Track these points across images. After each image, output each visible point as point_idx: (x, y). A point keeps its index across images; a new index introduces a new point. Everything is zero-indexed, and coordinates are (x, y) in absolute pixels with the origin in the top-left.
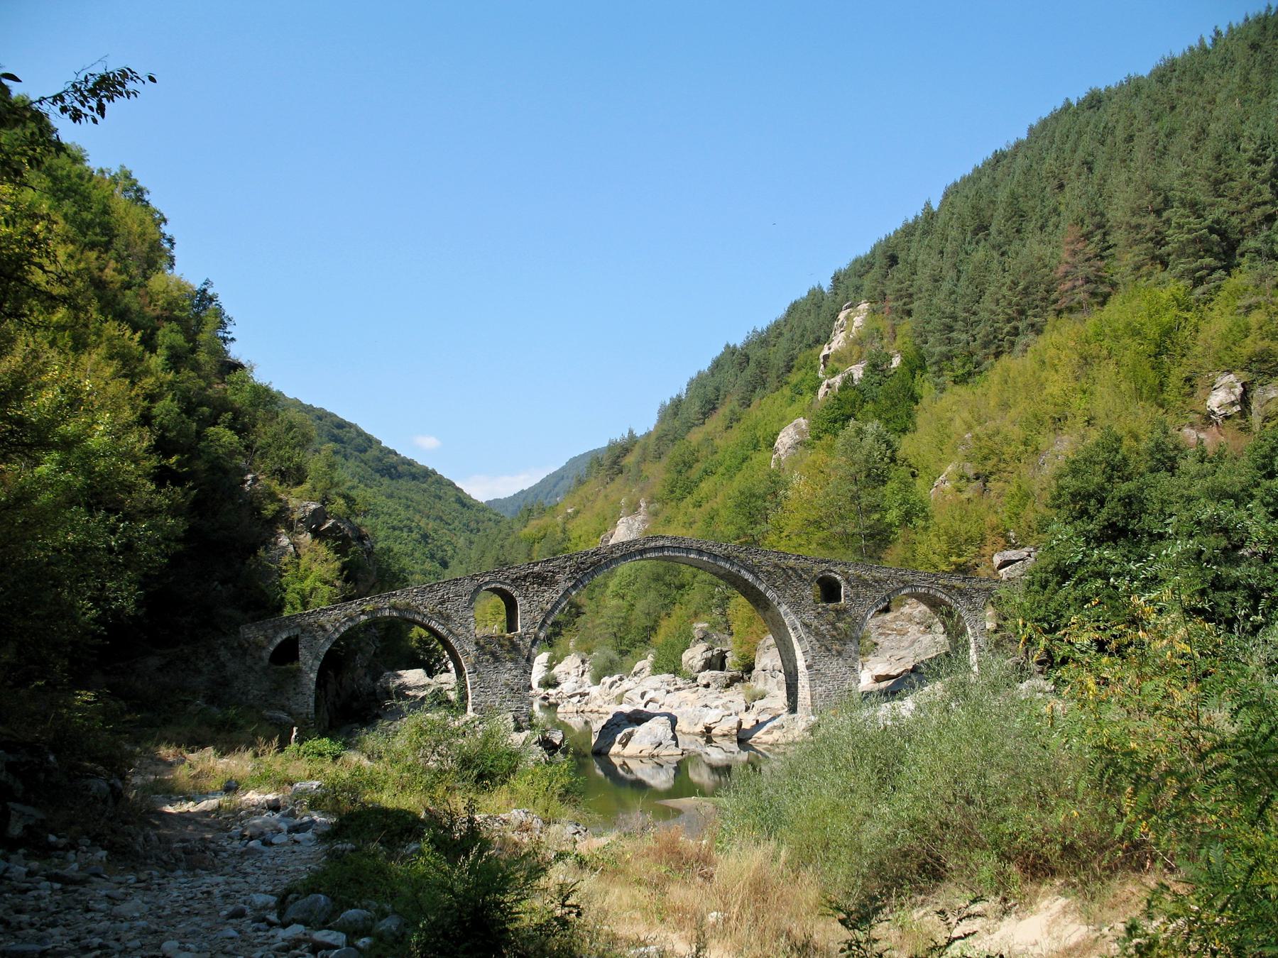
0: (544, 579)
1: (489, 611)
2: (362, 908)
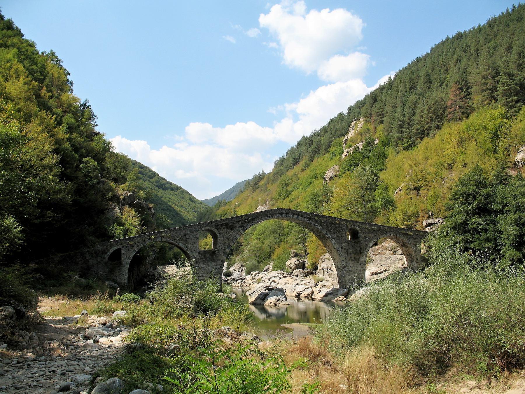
2: (143, 389)
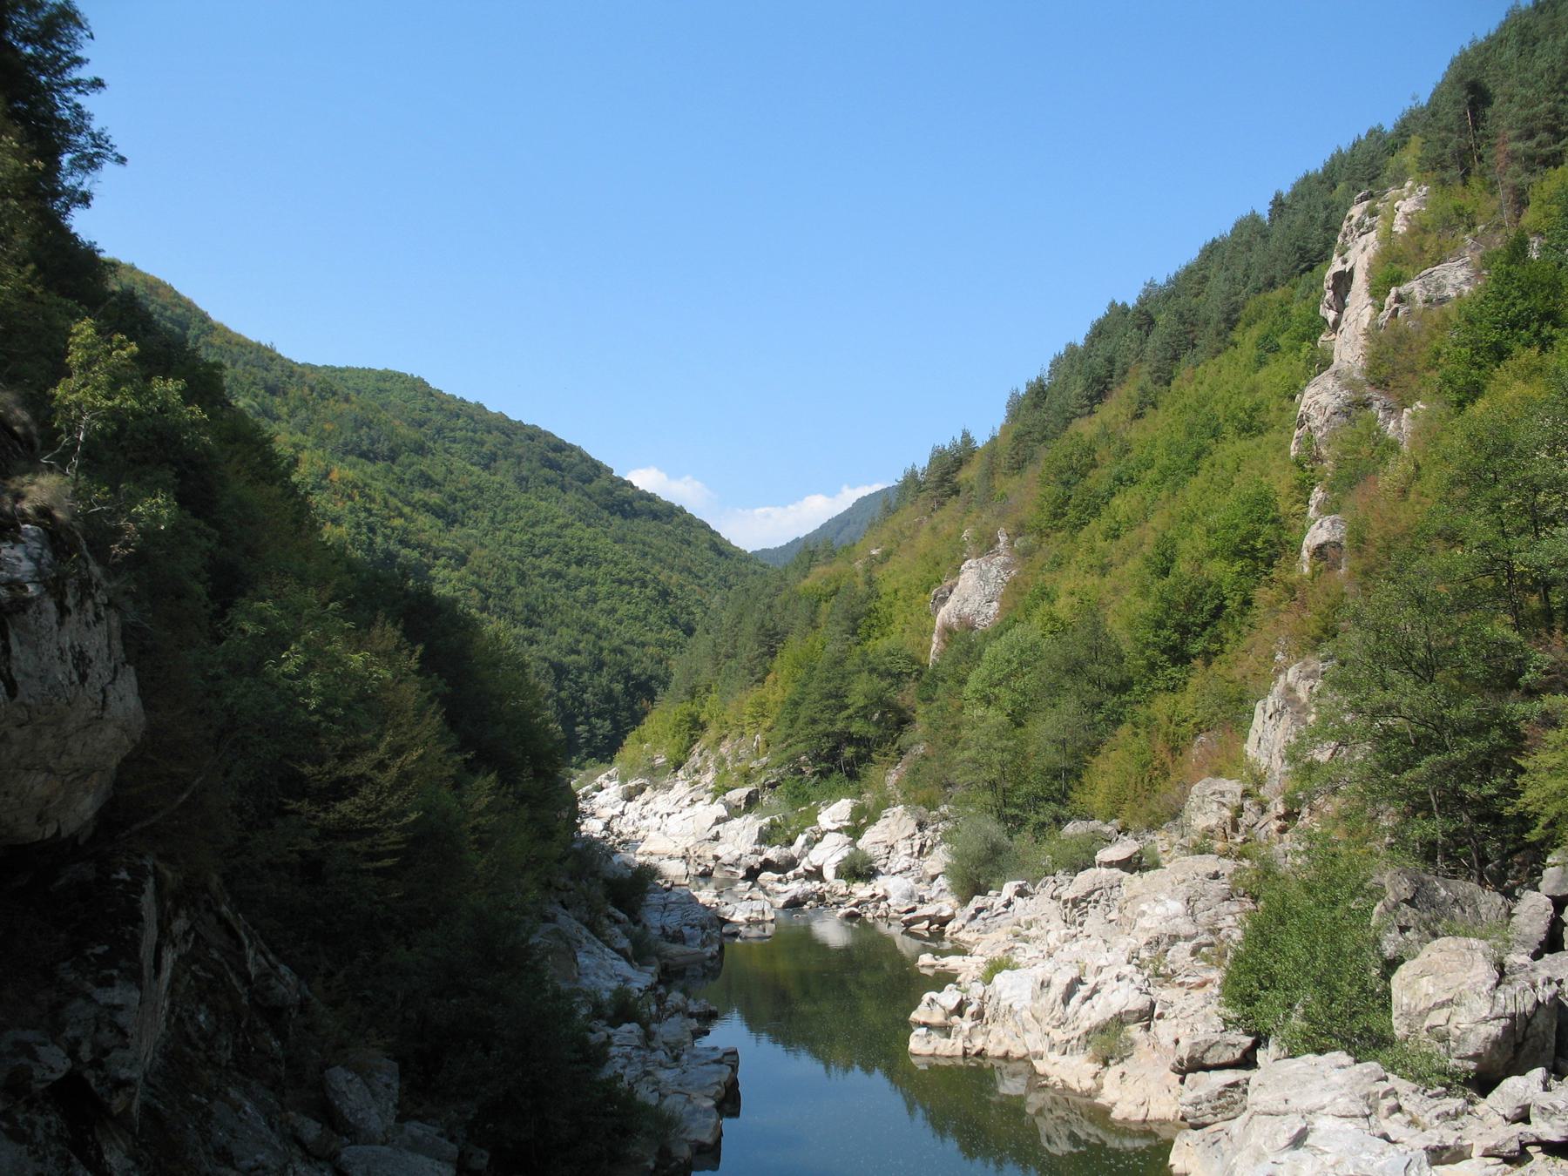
1: (748, 710)
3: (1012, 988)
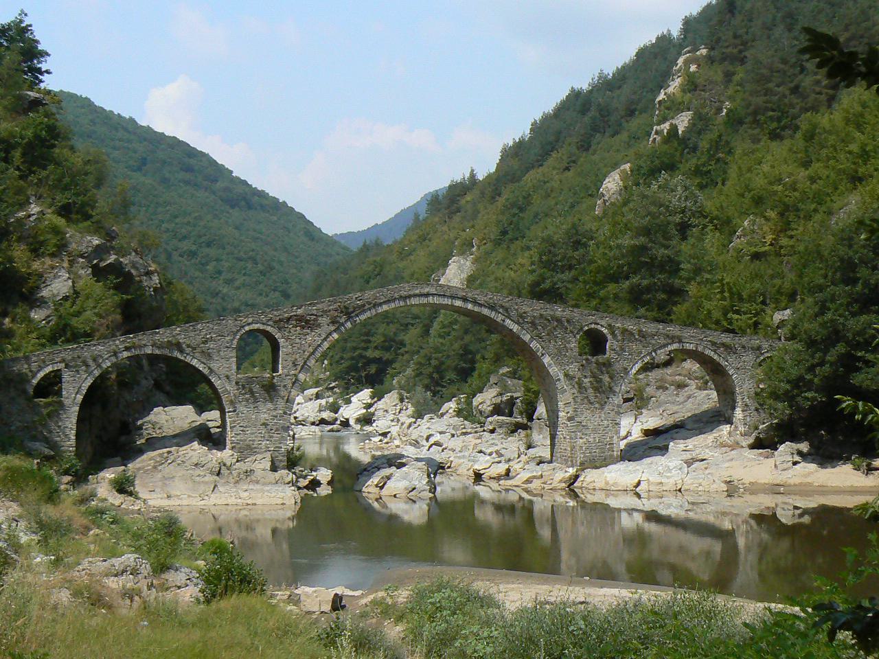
0: (307, 322)
3: (266, 286)
